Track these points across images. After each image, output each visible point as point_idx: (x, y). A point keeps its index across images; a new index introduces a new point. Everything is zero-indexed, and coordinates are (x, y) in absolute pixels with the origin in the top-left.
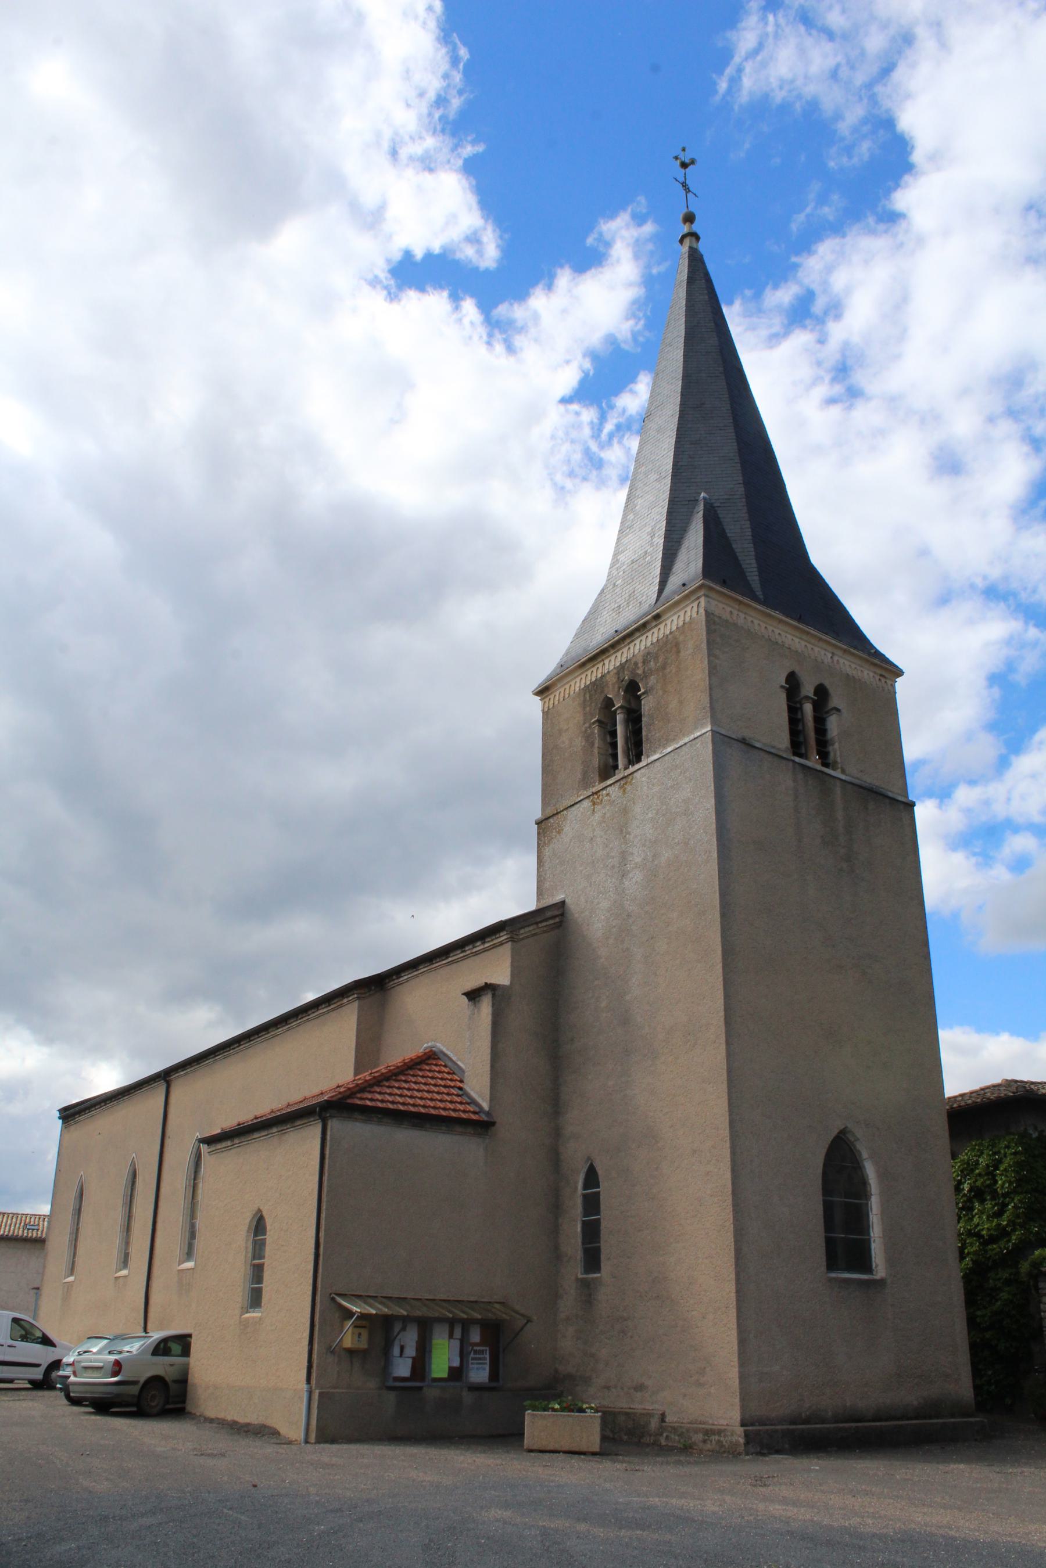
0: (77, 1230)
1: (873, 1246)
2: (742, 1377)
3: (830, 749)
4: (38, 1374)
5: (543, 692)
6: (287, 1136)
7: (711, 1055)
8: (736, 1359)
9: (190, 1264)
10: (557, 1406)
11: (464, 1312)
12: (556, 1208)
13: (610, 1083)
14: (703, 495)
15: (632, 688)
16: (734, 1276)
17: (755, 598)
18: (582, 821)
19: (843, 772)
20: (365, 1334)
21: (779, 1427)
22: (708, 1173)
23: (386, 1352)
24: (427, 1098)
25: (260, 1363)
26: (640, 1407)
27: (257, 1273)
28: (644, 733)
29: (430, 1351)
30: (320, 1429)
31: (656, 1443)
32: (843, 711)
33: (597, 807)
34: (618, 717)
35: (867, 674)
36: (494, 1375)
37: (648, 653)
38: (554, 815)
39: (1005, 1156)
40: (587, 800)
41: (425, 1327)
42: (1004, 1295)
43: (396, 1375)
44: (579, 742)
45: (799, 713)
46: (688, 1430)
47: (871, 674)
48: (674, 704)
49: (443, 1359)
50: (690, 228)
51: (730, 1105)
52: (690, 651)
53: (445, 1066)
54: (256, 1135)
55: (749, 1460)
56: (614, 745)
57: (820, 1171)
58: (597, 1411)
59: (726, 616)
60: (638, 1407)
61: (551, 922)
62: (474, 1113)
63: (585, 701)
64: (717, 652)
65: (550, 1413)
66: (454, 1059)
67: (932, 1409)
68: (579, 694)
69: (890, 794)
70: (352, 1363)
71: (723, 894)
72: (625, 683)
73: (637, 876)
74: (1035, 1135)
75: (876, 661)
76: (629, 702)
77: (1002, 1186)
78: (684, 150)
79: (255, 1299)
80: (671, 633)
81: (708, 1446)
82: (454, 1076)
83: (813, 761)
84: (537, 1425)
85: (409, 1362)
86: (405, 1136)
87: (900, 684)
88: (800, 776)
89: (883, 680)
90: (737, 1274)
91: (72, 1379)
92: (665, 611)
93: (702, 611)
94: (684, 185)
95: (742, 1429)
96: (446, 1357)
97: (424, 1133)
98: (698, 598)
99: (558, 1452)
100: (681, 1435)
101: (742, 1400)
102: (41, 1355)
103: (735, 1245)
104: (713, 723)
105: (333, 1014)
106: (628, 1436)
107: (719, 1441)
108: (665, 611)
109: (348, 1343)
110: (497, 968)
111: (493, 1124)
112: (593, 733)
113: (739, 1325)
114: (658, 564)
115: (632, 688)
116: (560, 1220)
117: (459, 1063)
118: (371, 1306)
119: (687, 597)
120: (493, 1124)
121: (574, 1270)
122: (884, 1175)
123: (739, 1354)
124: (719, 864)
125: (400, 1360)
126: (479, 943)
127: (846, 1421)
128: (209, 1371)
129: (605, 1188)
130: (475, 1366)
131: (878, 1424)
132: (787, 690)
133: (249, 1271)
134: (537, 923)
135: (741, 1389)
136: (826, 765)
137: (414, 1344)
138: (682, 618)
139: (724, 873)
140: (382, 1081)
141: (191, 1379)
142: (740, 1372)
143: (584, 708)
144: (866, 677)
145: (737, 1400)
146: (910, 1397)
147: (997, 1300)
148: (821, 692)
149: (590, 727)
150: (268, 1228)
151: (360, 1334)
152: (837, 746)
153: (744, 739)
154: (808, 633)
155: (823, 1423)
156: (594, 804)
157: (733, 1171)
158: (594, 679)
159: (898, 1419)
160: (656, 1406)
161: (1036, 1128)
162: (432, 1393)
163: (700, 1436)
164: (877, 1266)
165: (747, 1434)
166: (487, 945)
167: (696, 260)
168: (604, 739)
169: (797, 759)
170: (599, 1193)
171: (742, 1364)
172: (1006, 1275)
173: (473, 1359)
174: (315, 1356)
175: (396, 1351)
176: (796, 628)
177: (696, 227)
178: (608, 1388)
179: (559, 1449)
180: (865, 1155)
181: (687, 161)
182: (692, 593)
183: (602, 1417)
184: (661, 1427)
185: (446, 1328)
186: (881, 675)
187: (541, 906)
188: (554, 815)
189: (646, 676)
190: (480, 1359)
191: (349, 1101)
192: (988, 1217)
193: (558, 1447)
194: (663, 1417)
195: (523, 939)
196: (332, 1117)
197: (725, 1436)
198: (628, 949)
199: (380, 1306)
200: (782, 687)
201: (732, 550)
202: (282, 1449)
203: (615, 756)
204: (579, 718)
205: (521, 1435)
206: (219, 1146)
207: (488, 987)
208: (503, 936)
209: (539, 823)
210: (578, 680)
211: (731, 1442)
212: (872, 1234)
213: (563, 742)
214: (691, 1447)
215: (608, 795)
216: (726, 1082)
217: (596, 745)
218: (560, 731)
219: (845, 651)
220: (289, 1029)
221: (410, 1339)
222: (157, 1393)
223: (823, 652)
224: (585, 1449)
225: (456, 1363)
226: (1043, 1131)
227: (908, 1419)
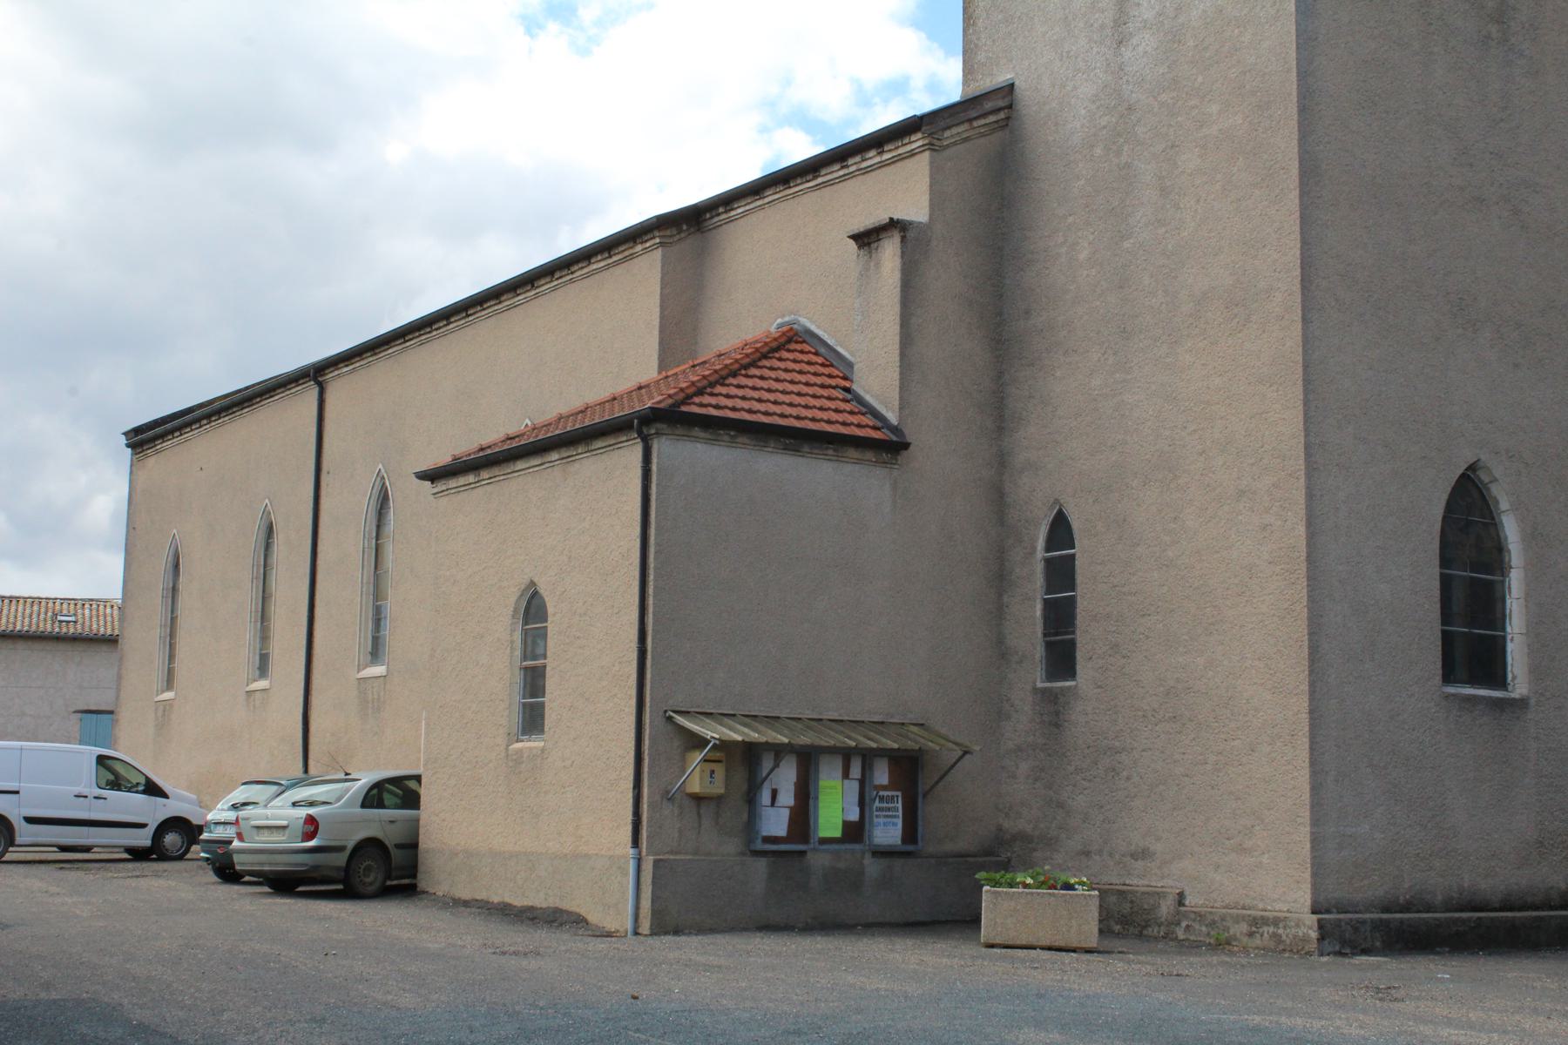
0: (173, 620)
1: (1510, 647)
2: (1316, 841)
4: (143, 839)
6: (577, 465)
7: (1276, 337)
9: (379, 670)
12: (1000, 579)
16: (1305, 687)
20: (720, 770)
21: (1367, 916)
22: (1264, 528)
23: (751, 799)
24: (752, 399)
25: (549, 813)
26: (1141, 882)
27: (534, 681)
29: (817, 798)
30: (656, 913)
36: (910, 833)
41: (808, 760)
46: (1223, 919)
49: (834, 807)
53: (816, 354)
54: (520, 465)
55: (1327, 963)
61: (992, 118)
62: (875, 428)
70: (699, 815)
73: (1144, 44)
79: (533, 720)
81: (1257, 941)
82: (834, 369)
84: (1000, 907)
85: (786, 813)
86: (771, 464)
90: (1312, 685)
91: (236, 843)
95: (1315, 917)
96: (839, 806)
99: (1074, 951)
101: (1314, 875)
102: (153, 812)
105: (618, 270)
106: (1129, 922)
107: (1275, 935)
109: (695, 787)
110: (905, 192)
111: (906, 446)
113: (1313, 763)
116: (1005, 599)
120: (906, 446)
121: (1032, 673)
122: (1532, 537)
123: (1312, 807)
124: (1298, 24)
125: (771, 811)
126: (872, 153)
127: (1462, 911)
128: (448, 826)
129: (1083, 551)
130: (881, 820)
131: (1509, 914)
133: (518, 678)
134: (970, 121)
135: (1313, 858)
137: (792, 788)
140: (724, 378)
141: (422, 846)
145: (1307, 875)
150: (550, 610)
151: (713, 772)
157: (1309, 524)
159: (1537, 908)
160: (1170, 882)
162: (819, 860)
163: (1244, 927)
164: (1514, 678)
165: (1321, 925)
166: (886, 156)
170: (1073, 557)
171: (1316, 821)
174: (645, 807)
175: (765, 797)
178: (1087, 854)
180: (1504, 505)
184: (1178, 913)
185: (838, 764)
187: (986, 83)
190: (889, 809)
191: (684, 409)
193: (1032, 941)
194: (1181, 899)
198: (1128, 165)
199: (746, 730)
202: (601, 945)
205: (973, 921)
206: (453, 483)
207: (893, 224)
208: (917, 141)
211: (1295, 937)
212: (1509, 629)
214: (1229, 943)
216: (1300, 383)
220: (536, 296)
221: (785, 778)
222: (375, 864)
224: (1075, 945)
225: (854, 816)
227: (1551, 908)
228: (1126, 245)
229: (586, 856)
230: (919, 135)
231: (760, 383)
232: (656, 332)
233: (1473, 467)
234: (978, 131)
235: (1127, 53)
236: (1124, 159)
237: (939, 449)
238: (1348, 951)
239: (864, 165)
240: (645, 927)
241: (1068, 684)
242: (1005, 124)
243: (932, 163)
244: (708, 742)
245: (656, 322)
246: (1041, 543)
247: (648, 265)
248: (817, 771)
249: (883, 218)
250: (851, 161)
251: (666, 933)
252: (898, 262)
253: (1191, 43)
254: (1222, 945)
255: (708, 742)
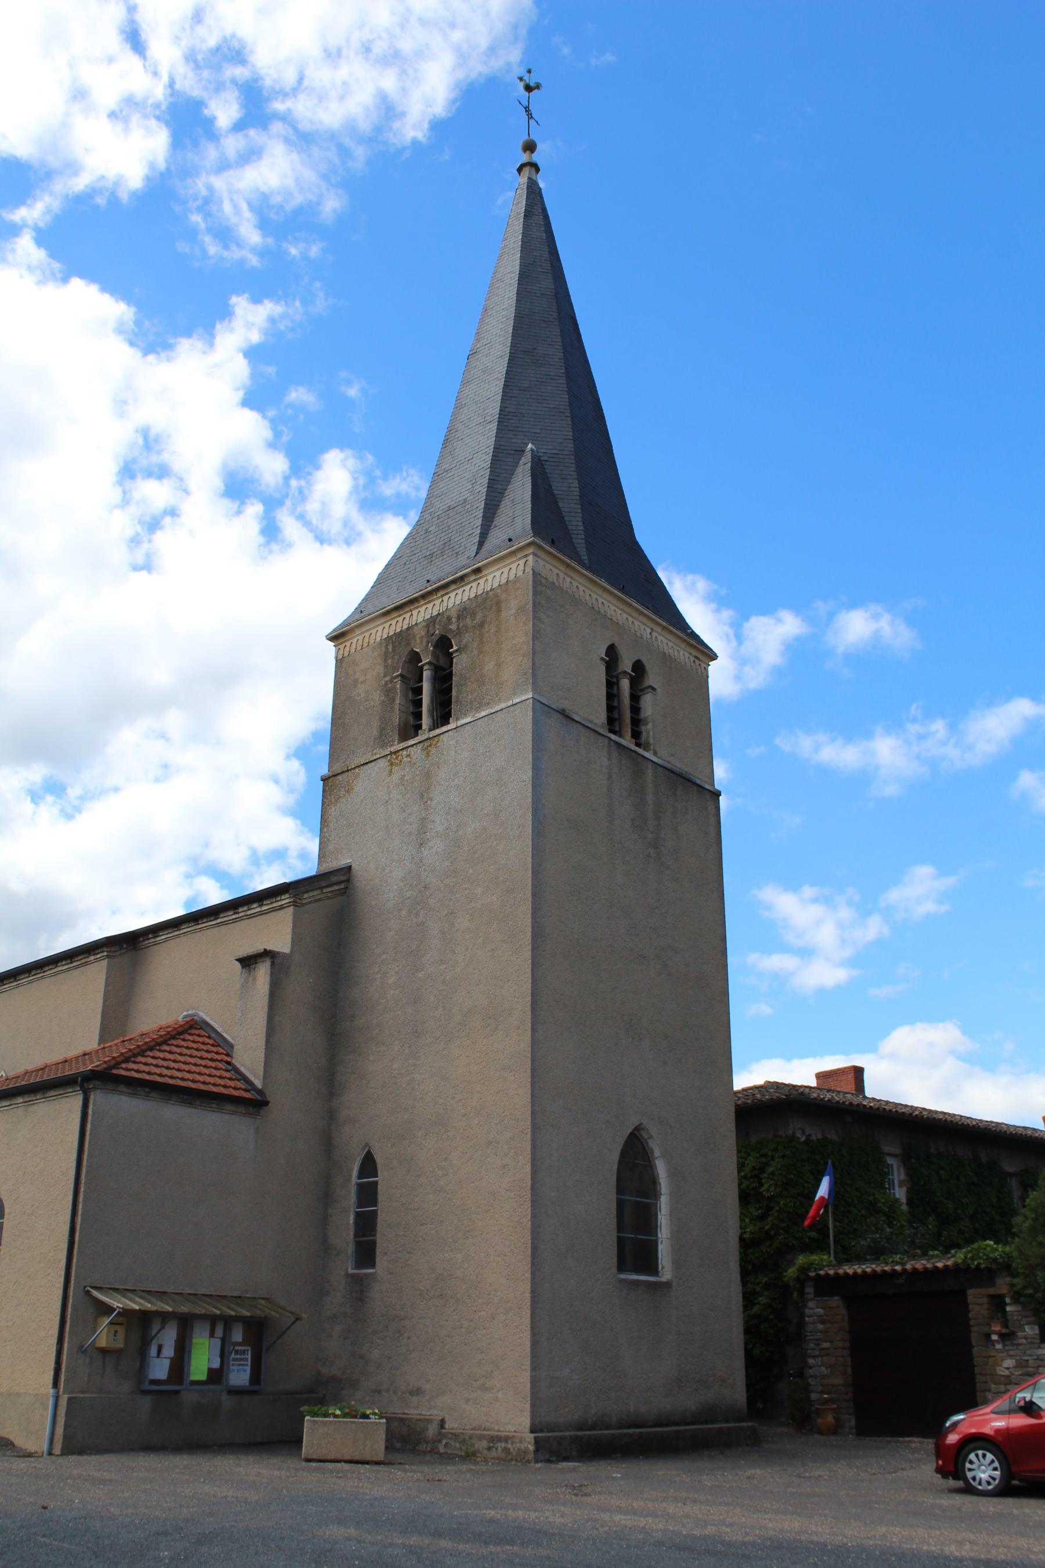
1: (660, 1247)
2: (534, 1382)
3: (643, 728)
5: (337, 637)
6: (35, 1107)
7: (514, 1041)
8: (529, 1363)
10: (338, 1412)
11: (216, 1308)
12: (327, 1197)
13: (396, 1065)
14: (530, 446)
15: (443, 645)
16: (528, 1275)
17: (581, 563)
18: (376, 783)
19: (655, 754)
20: (122, 1331)
21: (567, 1434)
22: (504, 1167)
23: (143, 1352)
28: (454, 694)
29: (190, 1352)
30: (67, 1438)
31: (434, 1451)
32: (659, 690)
33: (395, 769)
34: (425, 673)
35: (683, 654)
37: (465, 609)
38: (343, 772)
39: (773, 1158)
40: (383, 760)
41: (185, 1324)
42: (762, 1300)
43: (151, 1377)
44: (377, 697)
45: (615, 688)
46: (471, 1437)
47: (687, 655)
48: (489, 666)
49: (202, 1360)
50: (531, 157)
51: (532, 1096)
52: (513, 611)
53: (209, 1037)
56: (418, 703)
57: (615, 1167)
58: (381, 1417)
59: (552, 578)
60: (413, 1412)
61: (336, 888)
62: (246, 1090)
63: (386, 652)
64: (542, 616)
65: (331, 1419)
66: (219, 1030)
67: (709, 1414)
68: (380, 644)
69: (698, 782)
70: (104, 1363)
71: (536, 873)
72: (435, 638)
73: (437, 846)
74: (803, 1139)
75: (693, 642)
76: (438, 660)
77: (768, 1190)
78: (529, 72)
80: (491, 590)
81: (494, 1454)
82: (222, 1047)
83: (627, 741)
85: (166, 1363)
86: (172, 1112)
87: (713, 667)
88: (615, 754)
89: (697, 662)
90: (533, 1274)
92: (487, 566)
93: (529, 570)
94: (527, 110)
95: (532, 1435)
97: (193, 1110)
98: (526, 556)
100: (463, 1442)
101: (533, 1405)
103: (532, 1243)
104: (534, 691)
105: (76, 972)
106: (409, 1442)
108: (487, 566)
109: (103, 1343)
110: (276, 932)
111: (266, 1103)
112: (395, 688)
113: (532, 1328)
114: (480, 514)
115: (443, 645)
116: (329, 1211)
117: (225, 1035)
118: (131, 1300)
119: (513, 553)
120: (266, 1103)
122: (674, 1174)
125: (157, 1361)
126: (255, 905)
127: (629, 1427)
129: (383, 1179)
130: (235, 1368)
132: (607, 662)
134: (321, 888)
135: (532, 1394)
136: (638, 745)
138: (505, 575)
139: (538, 851)
142: (531, 1377)
143: (385, 660)
144: (682, 657)
145: (528, 1405)
146: (689, 1401)
147: (754, 1305)
148: (639, 667)
149: (391, 681)
150: (7, 1210)
151: (116, 1332)
152: (650, 726)
153: (564, 710)
154: (631, 606)
155: (607, 1429)
156: (392, 764)
157: (533, 1165)
158: (398, 630)
160: (434, 1412)
161: (803, 1133)
162: (189, 1397)
163: (484, 1444)
164: (663, 1268)
165: (537, 1441)
166: (264, 908)
167: (534, 194)
168: (406, 696)
169: (613, 737)
170: (376, 1183)
171: (534, 1368)
172: (765, 1280)
173: (235, 1360)
175: (153, 1351)
176: (619, 599)
177: (536, 157)
178: (379, 1392)
179: (341, 1458)
181: (532, 84)
182: (521, 549)
183: (387, 1423)
184: (440, 1433)
186: (696, 657)
188: (343, 772)
189: (459, 632)
190: (241, 1360)
191: (115, 1071)
192: (751, 1220)
193: (339, 1456)
195: (306, 904)
196: (95, 1088)
197: (512, 1443)
198: (423, 923)
199: (142, 1302)
200: (602, 659)
201: (559, 508)
203: (418, 716)
204: (380, 669)
205: (300, 1441)
207: (267, 954)
208: (285, 899)
209: (324, 779)
210: (380, 628)
212: (659, 1235)
213: (359, 695)
215: (408, 756)
216: (529, 1071)
217: (398, 701)
218: (356, 682)
219: (664, 628)
220: (17, 986)
221: (169, 1337)
223: (642, 627)
224: (368, 1459)
225: (216, 1364)
226: (810, 1135)
227: (687, 1424)
228: (420, 975)
229: (18, 1394)
230: (287, 896)
231: (168, 1056)
232: (99, 1017)
233: (638, 1128)
234: (326, 896)
235: (425, 852)
236: (421, 919)
237: (290, 1107)
238: (554, 1459)
239: (249, 912)
240: (58, 1449)
241: (370, 1271)
242: (345, 892)
243: (295, 915)
244: (114, 1310)
245: (100, 1010)
246: (355, 1173)
247: (97, 971)
248: (191, 1338)
249: (259, 948)
250: (240, 910)
251: (73, 1453)
252: (268, 979)
253: (466, 848)
254: (469, 1456)
255: (114, 1310)
